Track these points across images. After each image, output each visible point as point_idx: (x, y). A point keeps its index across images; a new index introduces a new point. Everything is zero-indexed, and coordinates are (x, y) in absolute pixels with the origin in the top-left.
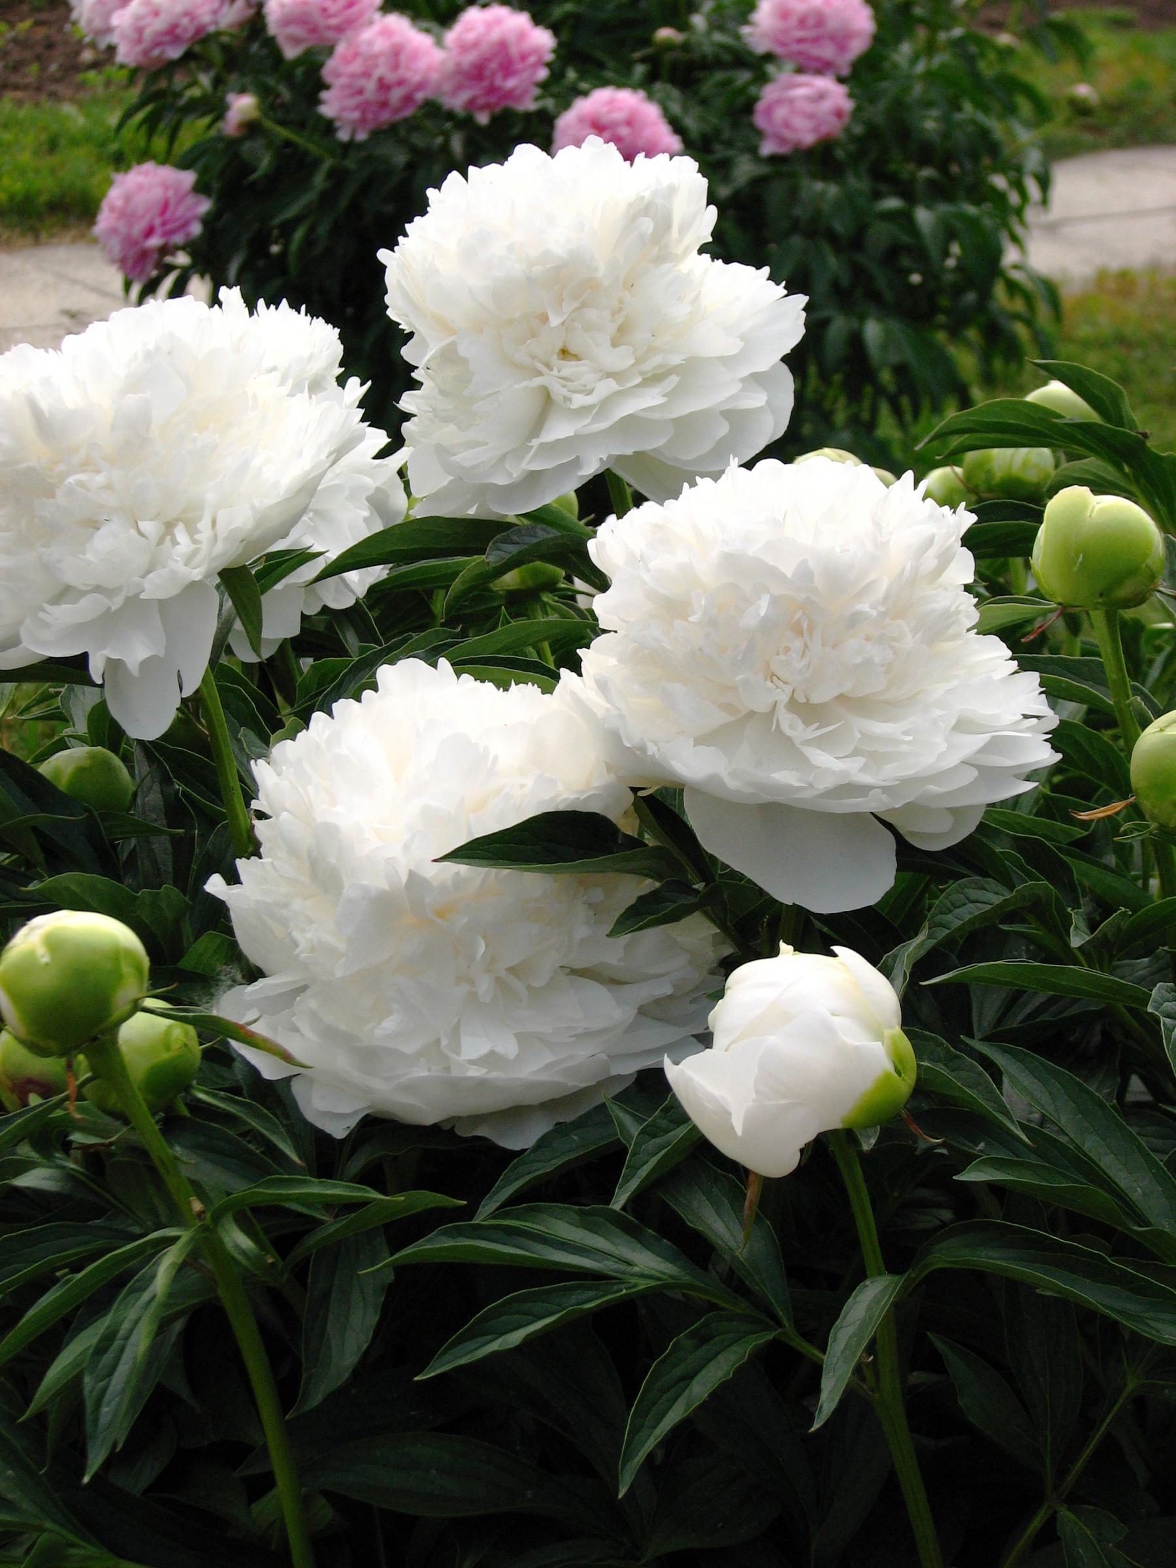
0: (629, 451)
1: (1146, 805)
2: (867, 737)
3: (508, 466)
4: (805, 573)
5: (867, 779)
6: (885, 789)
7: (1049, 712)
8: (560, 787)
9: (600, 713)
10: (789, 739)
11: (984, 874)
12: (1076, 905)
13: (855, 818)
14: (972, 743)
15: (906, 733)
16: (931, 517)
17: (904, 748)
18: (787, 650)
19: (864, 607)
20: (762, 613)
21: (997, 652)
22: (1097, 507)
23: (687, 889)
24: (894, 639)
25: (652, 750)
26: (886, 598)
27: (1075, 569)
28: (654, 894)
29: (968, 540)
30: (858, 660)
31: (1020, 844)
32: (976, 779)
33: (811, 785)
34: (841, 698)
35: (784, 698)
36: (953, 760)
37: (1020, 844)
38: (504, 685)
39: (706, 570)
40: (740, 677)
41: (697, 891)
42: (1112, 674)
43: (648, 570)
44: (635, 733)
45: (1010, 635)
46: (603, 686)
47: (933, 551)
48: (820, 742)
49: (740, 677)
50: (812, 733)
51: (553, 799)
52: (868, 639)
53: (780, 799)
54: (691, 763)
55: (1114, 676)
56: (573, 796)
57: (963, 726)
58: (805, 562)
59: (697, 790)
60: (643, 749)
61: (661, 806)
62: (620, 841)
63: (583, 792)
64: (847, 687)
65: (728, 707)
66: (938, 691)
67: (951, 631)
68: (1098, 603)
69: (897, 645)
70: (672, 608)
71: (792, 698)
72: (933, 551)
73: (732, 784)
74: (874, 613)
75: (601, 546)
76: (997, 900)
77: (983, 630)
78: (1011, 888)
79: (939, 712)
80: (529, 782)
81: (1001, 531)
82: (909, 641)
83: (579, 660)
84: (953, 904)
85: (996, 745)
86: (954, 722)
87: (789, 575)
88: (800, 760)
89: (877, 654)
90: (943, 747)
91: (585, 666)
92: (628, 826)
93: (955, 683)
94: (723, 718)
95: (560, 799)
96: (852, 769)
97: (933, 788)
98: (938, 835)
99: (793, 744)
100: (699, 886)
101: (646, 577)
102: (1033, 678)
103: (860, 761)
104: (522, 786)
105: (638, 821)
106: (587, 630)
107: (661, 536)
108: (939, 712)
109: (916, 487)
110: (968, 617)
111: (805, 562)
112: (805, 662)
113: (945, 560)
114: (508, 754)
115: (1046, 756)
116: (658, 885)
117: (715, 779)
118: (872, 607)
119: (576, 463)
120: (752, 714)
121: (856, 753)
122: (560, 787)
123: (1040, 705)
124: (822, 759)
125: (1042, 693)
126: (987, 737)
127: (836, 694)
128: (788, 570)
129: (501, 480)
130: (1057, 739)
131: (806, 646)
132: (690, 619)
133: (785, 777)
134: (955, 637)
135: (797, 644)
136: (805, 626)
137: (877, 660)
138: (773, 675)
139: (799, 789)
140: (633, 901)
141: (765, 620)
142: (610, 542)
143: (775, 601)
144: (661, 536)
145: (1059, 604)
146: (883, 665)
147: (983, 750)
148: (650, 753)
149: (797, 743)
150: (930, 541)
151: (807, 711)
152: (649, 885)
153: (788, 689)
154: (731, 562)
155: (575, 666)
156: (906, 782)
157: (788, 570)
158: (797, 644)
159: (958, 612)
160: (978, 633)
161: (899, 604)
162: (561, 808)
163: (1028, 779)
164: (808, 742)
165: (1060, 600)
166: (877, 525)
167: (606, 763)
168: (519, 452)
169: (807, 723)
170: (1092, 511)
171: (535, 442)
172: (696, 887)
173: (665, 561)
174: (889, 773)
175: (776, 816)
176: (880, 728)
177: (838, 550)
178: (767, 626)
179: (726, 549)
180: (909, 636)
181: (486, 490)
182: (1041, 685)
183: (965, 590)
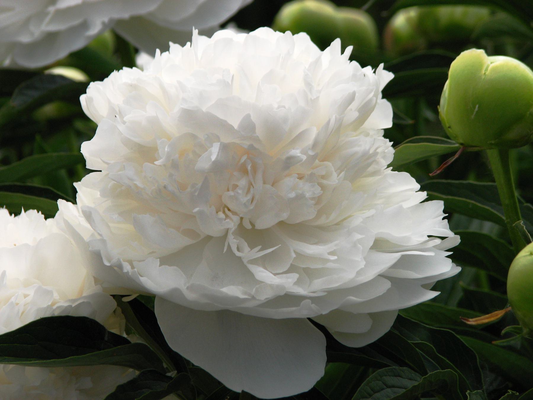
0: (126, 15)
1: (519, 314)
2: (300, 256)
3: (32, 28)
4: (248, 126)
5: (300, 291)
6: (315, 300)
7: (450, 234)
8: (56, 296)
9: (86, 237)
10: (240, 258)
11: (402, 364)
12: (478, 384)
13: (292, 325)
14: (386, 261)
15: (332, 253)
16: (354, 77)
17: (330, 265)
18: (235, 186)
19: (296, 152)
20: (213, 158)
21: (407, 187)
22: (491, 66)
23: (161, 376)
24: (323, 177)
25: (127, 268)
26: (315, 145)
27: (473, 117)
28: (132, 385)
29: (389, 93)
30: (292, 195)
31: (434, 335)
32: (389, 290)
33: (253, 298)
34: (281, 224)
35: (232, 224)
36: (370, 275)
37: (434, 335)
38: (15, 211)
39: (170, 123)
40: (196, 210)
41: (170, 378)
42: (505, 199)
43: (124, 123)
44: (115, 253)
45: (419, 169)
46: (88, 215)
47: (354, 106)
48: (264, 262)
49: (196, 210)
50: (256, 253)
51: (49, 307)
52: (301, 178)
53: (230, 307)
54: (158, 279)
55: (507, 202)
56: (66, 304)
57: (380, 245)
58: (248, 116)
59: (164, 299)
60: (120, 267)
61: (140, 308)
62: (106, 338)
63: (74, 301)
64: (284, 216)
65: (190, 233)
66: (358, 220)
67: (371, 169)
68: (491, 144)
69: (324, 182)
70: (144, 152)
71: (241, 226)
72: (354, 106)
73: (191, 296)
74: (304, 158)
75: (90, 100)
76: (410, 384)
77: (398, 166)
78: (424, 372)
79: (358, 236)
80: (31, 292)
81: (414, 87)
82: (334, 179)
83: (75, 191)
84: (372, 390)
85: (406, 261)
86: (371, 244)
87: (236, 126)
88: (248, 277)
89: (309, 190)
90: (362, 264)
91: (80, 196)
92: (115, 326)
93: (372, 212)
94: (185, 241)
95: (54, 307)
96: (288, 283)
97: (353, 298)
98: (360, 335)
99: (243, 262)
100: (172, 374)
101: (121, 128)
102: (438, 206)
103: (295, 276)
104: (26, 296)
105: (124, 321)
106: (77, 168)
107: (136, 95)
108: (358, 236)
109: (343, 52)
110: (384, 157)
111: (248, 116)
112: (249, 197)
113: (366, 111)
114: (15, 270)
115: (447, 268)
116: (137, 373)
117: (176, 291)
118: (304, 152)
119: (85, 26)
120: (209, 238)
121: (292, 269)
122: (56, 296)
123: (443, 228)
124: (263, 275)
125: (443, 219)
126: (398, 255)
127: (277, 221)
128: (235, 123)
129: (25, 39)
130: (457, 255)
131: (251, 184)
132: (156, 163)
133: (233, 290)
134: (375, 173)
135: (243, 182)
136: (249, 168)
137: (308, 195)
138: (226, 206)
139: (244, 300)
140: (112, 390)
141: (215, 162)
142: (100, 99)
143: (224, 147)
144: (136, 95)
145: (462, 144)
146: (313, 199)
147: (395, 266)
148: (125, 271)
149: (245, 261)
150: (352, 98)
151: (254, 235)
152: (131, 374)
153: (236, 219)
154: (190, 116)
155: (71, 196)
156: (332, 293)
157: (235, 123)
158: (243, 182)
159: (375, 154)
160: (392, 170)
161: (328, 148)
162: (57, 314)
163: (434, 289)
164: (254, 262)
165: (461, 141)
166: (308, 84)
167: (94, 277)
168: (40, 16)
169: (252, 247)
170: (487, 69)
171: (52, 9)
172: (169, 374)
173: (136, 115)
174: (319, 285)
175: (229, 320)
176: (312, 249)
177: (276, 106)
178: (218, 168)
179: (185, 106)
180: (335, 174)
181: (15, 47)
182: (445, 212)
183: (385, 136)
